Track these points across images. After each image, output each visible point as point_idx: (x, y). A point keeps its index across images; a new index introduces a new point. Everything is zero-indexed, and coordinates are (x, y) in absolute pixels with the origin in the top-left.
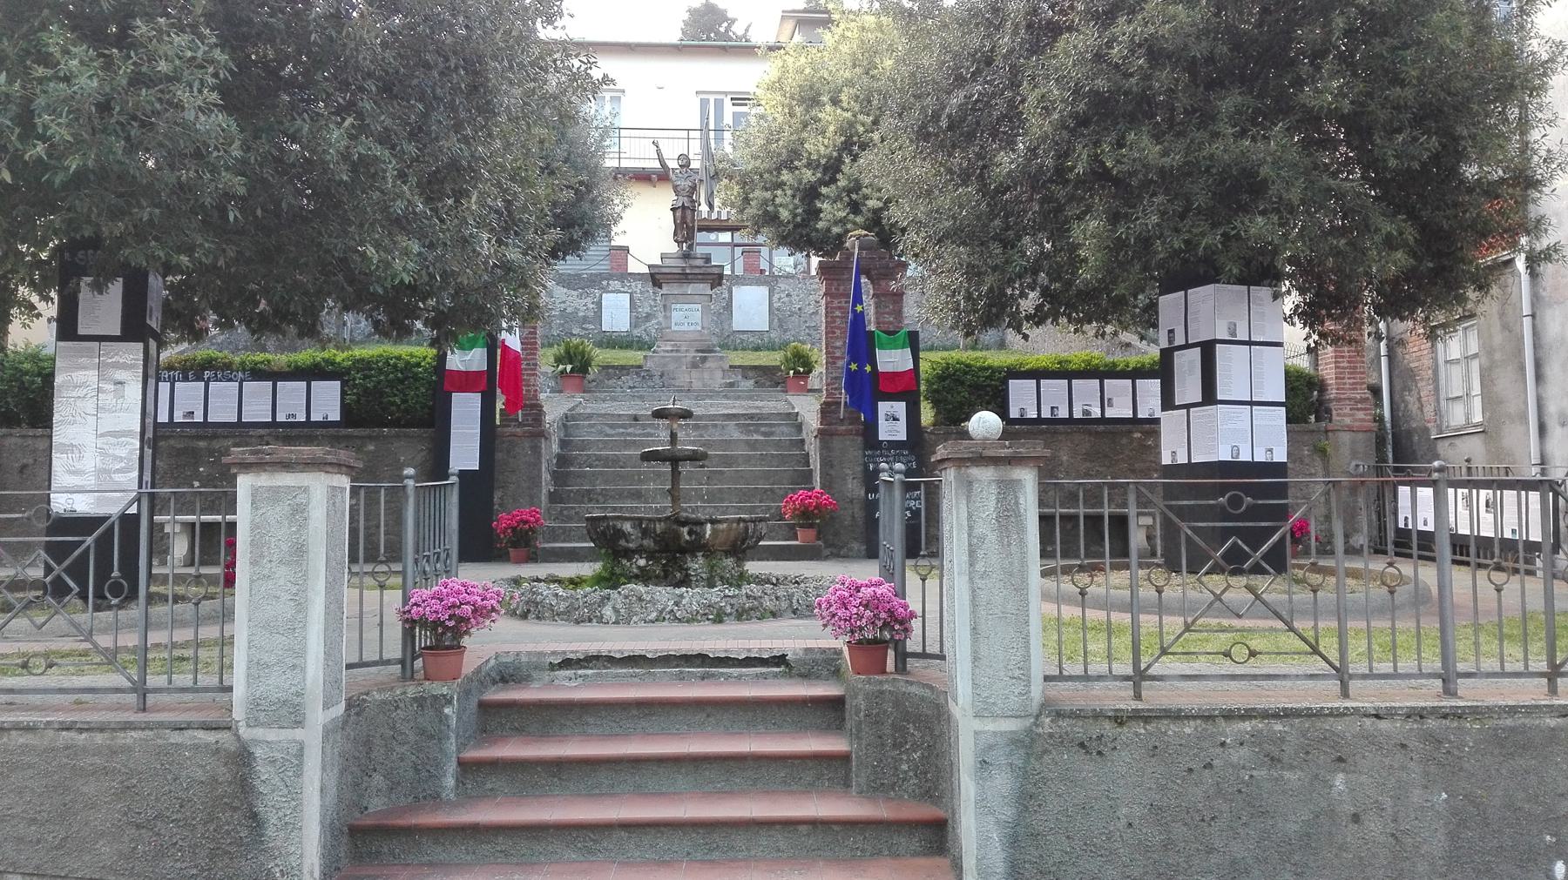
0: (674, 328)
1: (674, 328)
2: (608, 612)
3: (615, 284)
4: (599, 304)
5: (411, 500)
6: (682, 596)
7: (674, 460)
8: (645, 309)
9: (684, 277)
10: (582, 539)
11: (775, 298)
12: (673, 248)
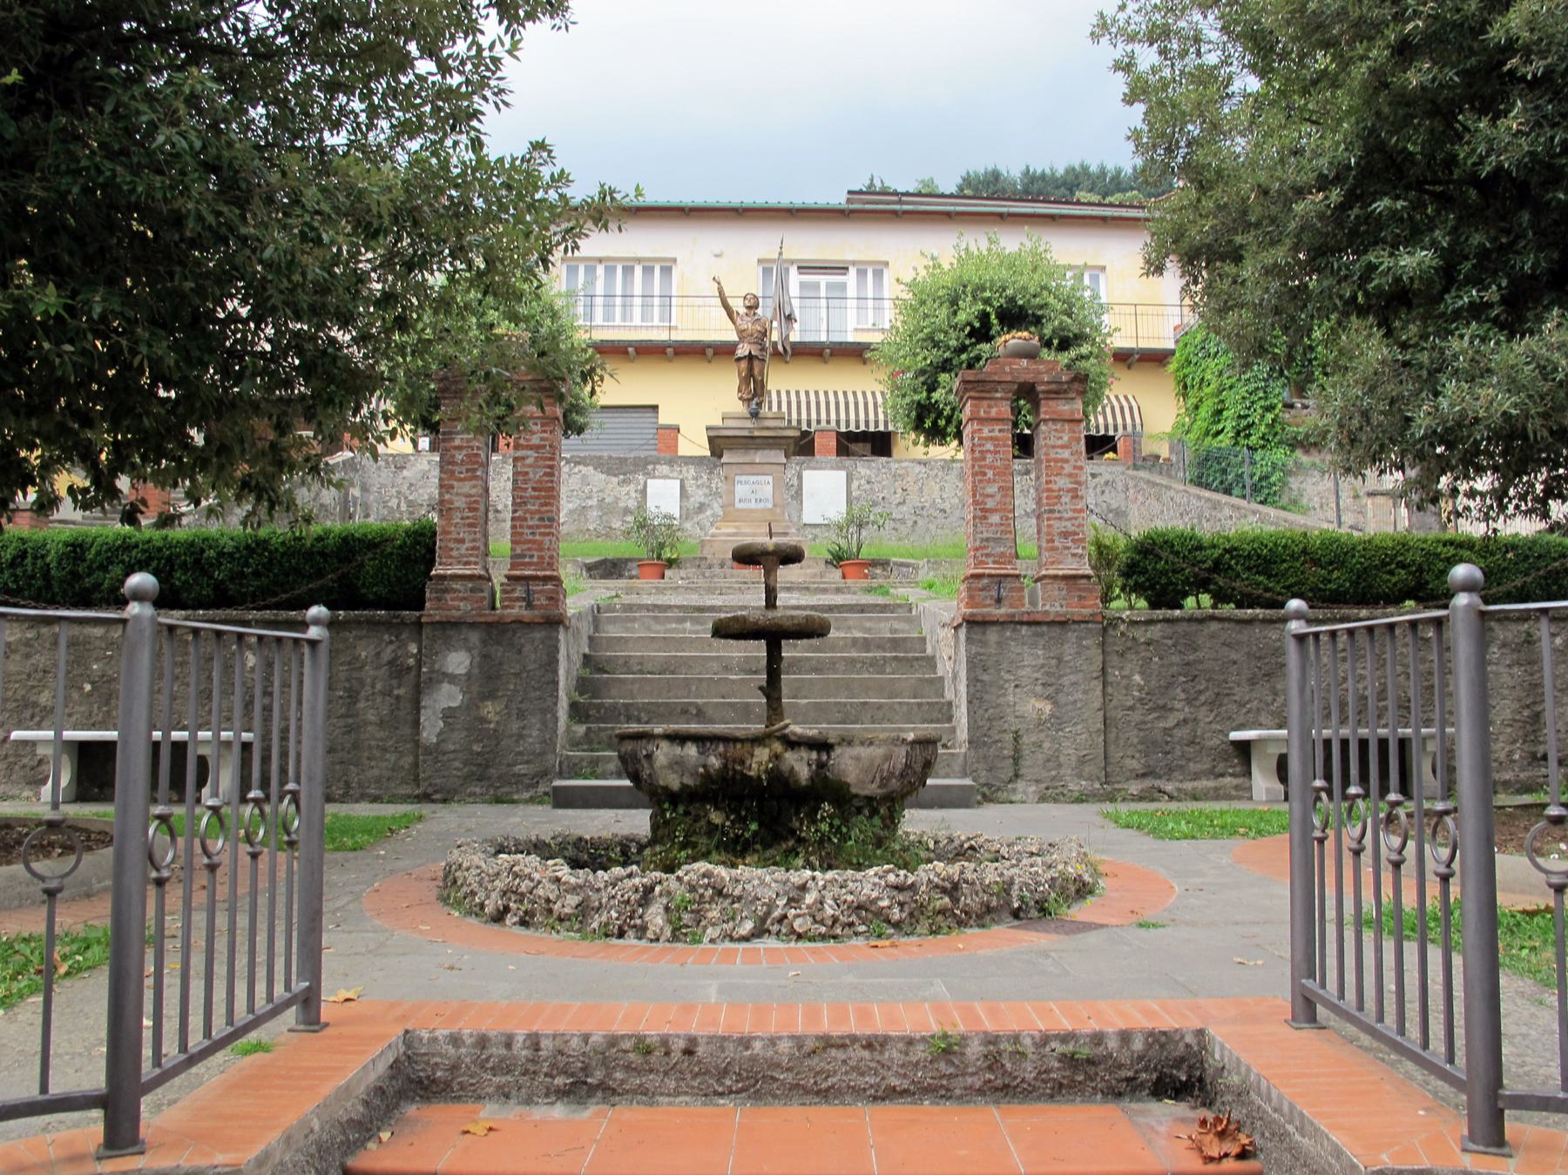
0: (738, 505)
1: (738, 505)
2: (655, 917)
3: (665, 469)
4: (644, 492)
5: (144, 657)
6: (803, 888)
7: (774, 636)
8: (698, 496)
9: (748, 443)
10: (619, 776)
11: (855, 484)
12: (739, 408)
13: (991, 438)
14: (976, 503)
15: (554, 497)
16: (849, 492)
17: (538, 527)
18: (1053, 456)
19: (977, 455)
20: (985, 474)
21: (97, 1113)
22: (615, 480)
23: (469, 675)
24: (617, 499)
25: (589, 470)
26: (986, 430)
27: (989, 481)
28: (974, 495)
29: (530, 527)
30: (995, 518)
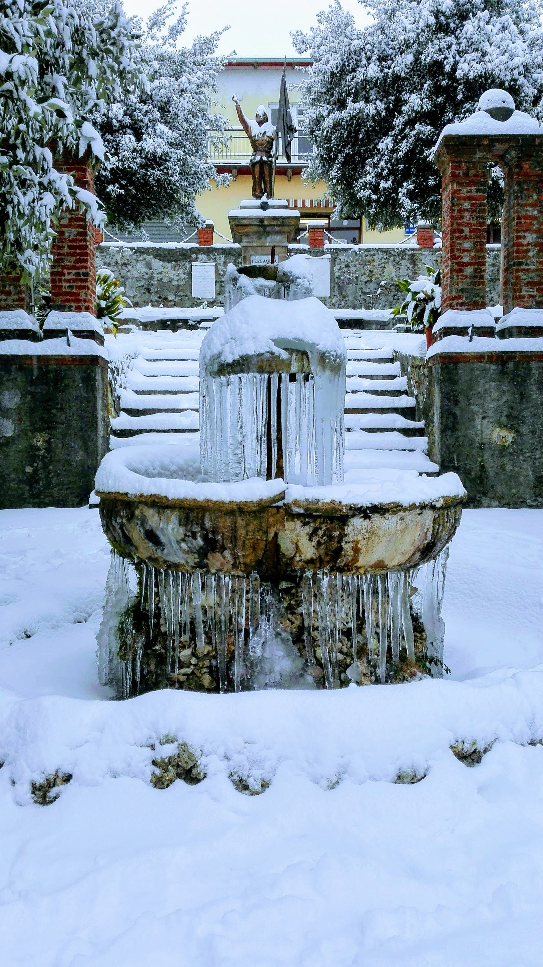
4: (190, 274)
11: (337, 267)
13: (470, 199)
14: (453, 257)
15: (87, 254)
16: (332, 273)
17: (75, 281)
18: (523, 213)
19: (456, 214)
20: (462, 231)
21: (97, 510)
22: (169, 265)
23: (18, 410)
24: (171, 280)
25: (149, 258)
26: (465, 190)
27: (465, 238)
28: (452, 251)
29: (67, 281)
30: (469, 270)
